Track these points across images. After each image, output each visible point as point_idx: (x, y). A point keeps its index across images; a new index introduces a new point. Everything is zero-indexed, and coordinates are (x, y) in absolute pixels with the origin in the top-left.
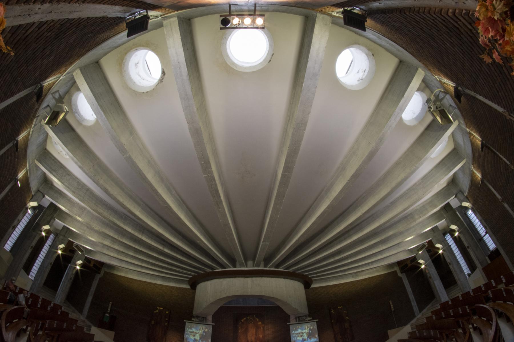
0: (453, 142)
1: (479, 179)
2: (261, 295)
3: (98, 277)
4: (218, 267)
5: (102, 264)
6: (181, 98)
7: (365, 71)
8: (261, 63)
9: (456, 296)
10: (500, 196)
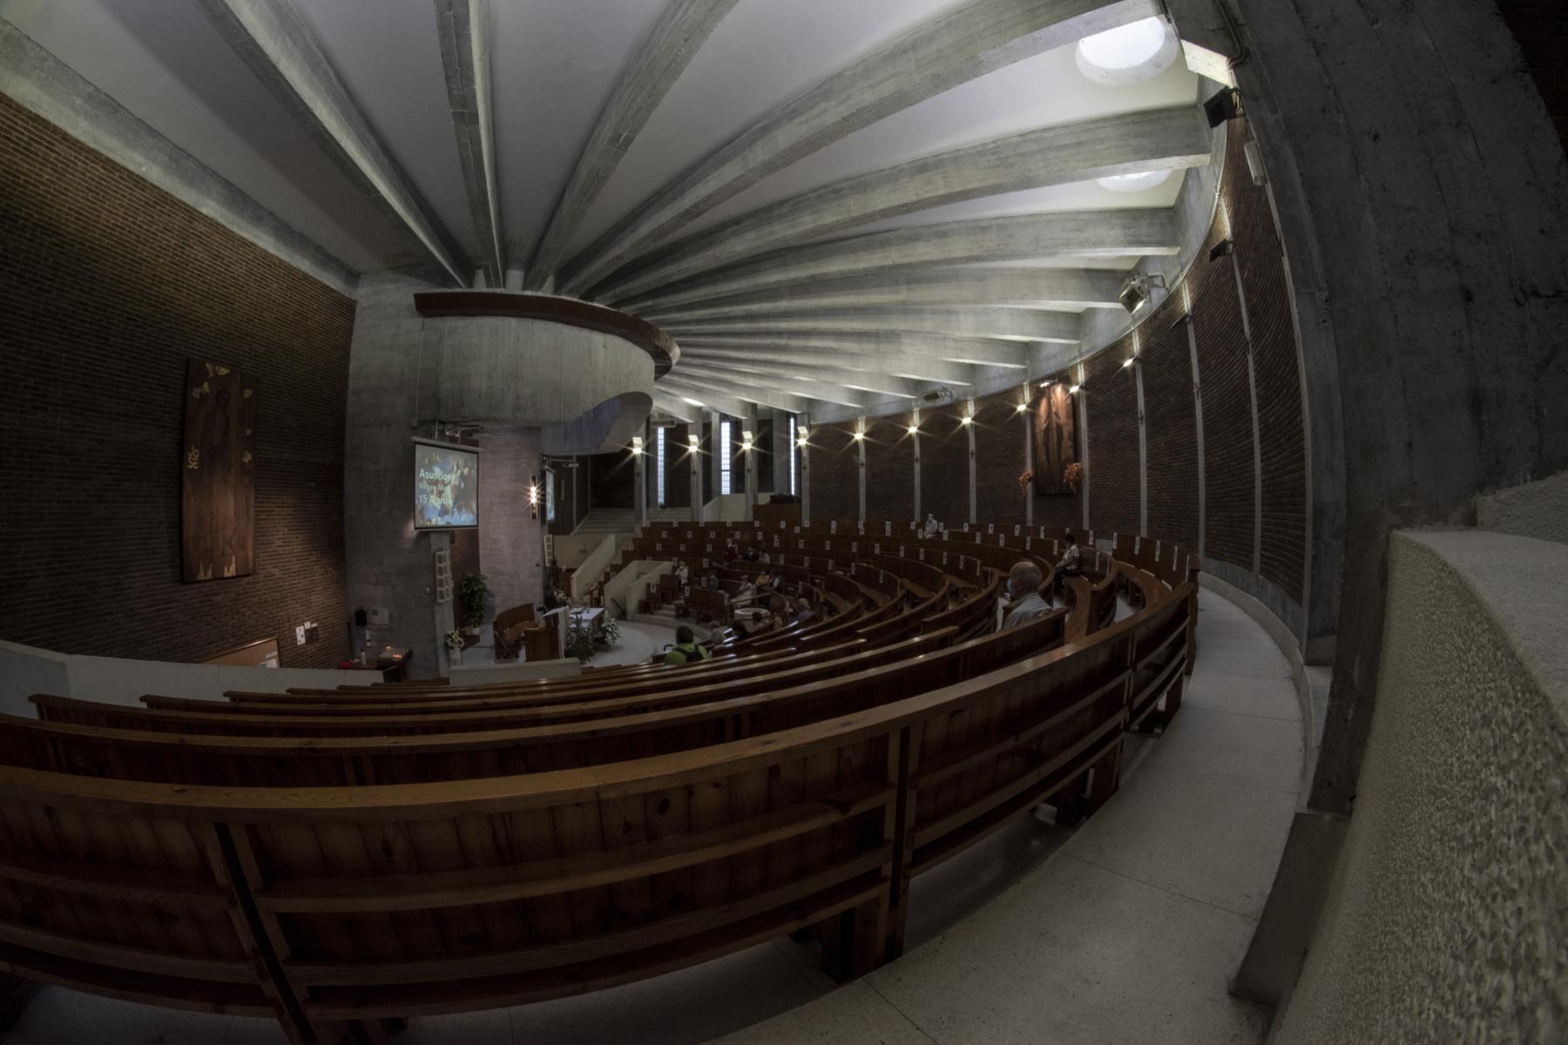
9: (671, 520)
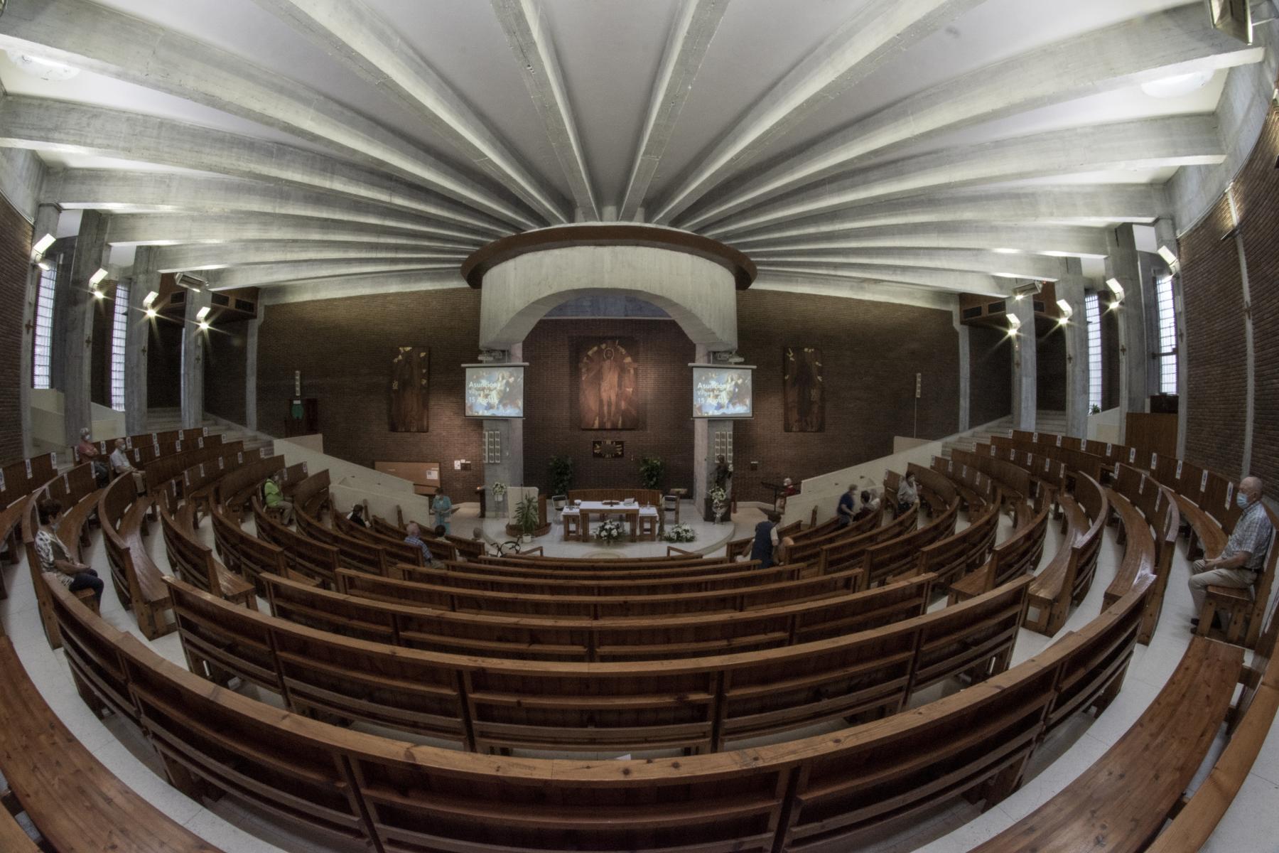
0: (1220, 94)
1: (1230, 225)
2: (633, 288)
3: (254, 326)
4: (532, 222)
5: (254, 292)
9: (1054, 434)
10: (1251, 296)
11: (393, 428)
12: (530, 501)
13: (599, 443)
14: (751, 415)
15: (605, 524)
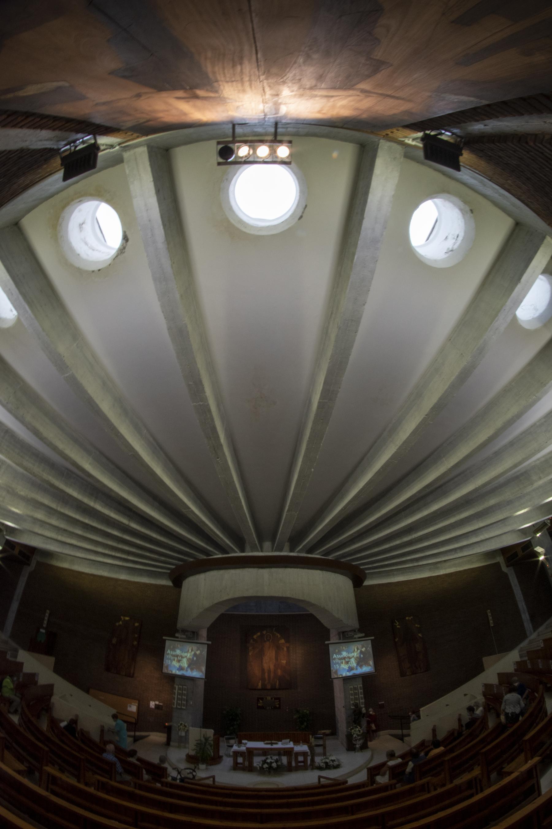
2: (284, 596)
3: (27, 571)
5: (33, 550)
6: (155, 279)
7: (457, 237)
8: (286, 220)
11: (108, 669)
12: (206, 739)
13: (262, 699)
14: (374, 671)
15: (267, 759)
